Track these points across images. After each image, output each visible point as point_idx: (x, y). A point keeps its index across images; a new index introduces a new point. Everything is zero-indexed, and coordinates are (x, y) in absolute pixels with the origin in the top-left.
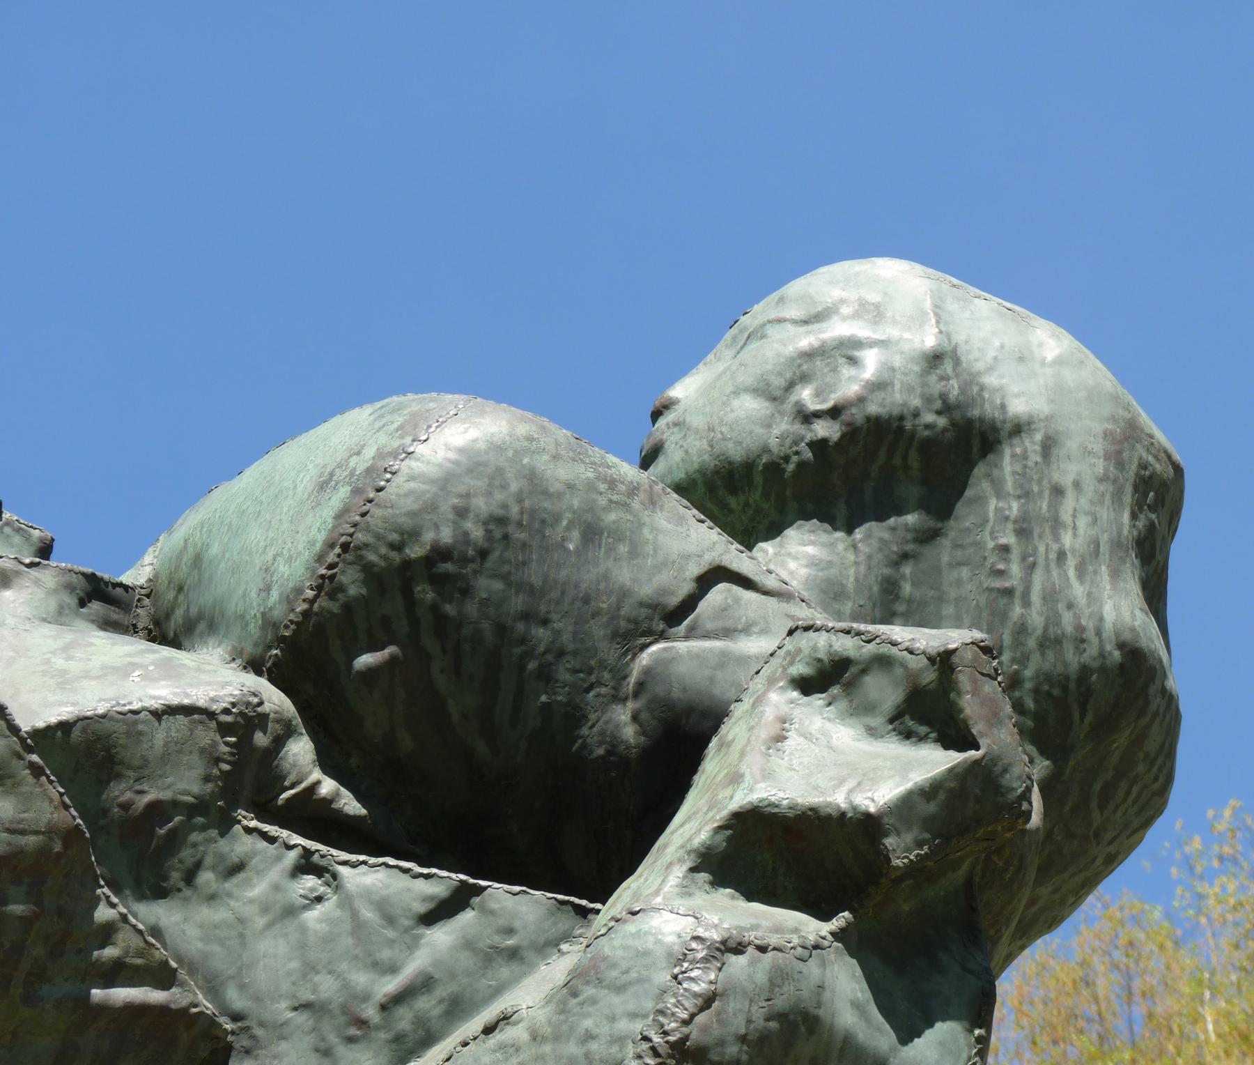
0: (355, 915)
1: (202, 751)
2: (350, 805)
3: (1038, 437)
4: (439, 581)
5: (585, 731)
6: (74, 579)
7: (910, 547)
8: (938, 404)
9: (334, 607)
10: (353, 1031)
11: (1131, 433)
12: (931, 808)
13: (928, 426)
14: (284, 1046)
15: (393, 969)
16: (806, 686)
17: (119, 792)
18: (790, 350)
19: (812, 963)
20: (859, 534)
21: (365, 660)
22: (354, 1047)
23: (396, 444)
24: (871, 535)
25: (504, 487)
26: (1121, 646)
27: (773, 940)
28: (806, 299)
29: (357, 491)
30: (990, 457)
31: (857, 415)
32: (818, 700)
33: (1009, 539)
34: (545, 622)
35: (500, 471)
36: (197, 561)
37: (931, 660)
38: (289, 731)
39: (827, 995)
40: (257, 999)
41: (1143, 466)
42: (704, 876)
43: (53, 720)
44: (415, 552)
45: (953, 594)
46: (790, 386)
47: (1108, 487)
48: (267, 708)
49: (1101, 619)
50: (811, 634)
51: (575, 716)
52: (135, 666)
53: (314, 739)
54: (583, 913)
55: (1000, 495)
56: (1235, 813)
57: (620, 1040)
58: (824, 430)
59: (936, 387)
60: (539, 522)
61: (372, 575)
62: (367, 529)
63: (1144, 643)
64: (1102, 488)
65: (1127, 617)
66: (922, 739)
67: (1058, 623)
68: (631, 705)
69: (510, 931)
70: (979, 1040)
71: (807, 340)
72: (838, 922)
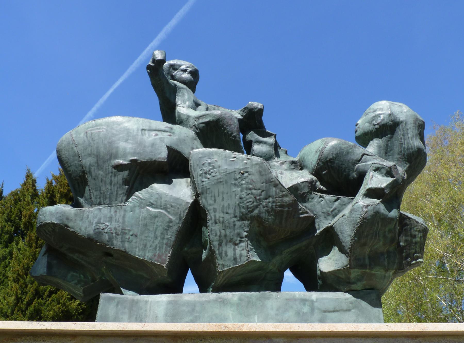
0: (327, 202)
1: (307, 186)
2: (325, 189)
3: (404, 123)
4: (331, 162)
5: (350, 176)
6: (290, 162)
7: (389, 139)
8: (391, 121)
9: (319, 167)
10: (328, 215)
11: (417, 119)
12: (390, 186)
13: (390, 124)
14: (321, 217)
15: (331, 208)
16: (375, 171)
17: (299, 192)
18: (371, 116)
19: (378, 205)
20: (383, 139)
21: (324, 172)
22: (329, 216)
23: (324, 146)
24: (384, 139)
25: (337, 150)
26: (417, 148)
27: (373, 204)
28: (373, 109)
29: (320, 153)
30: (398, 126)
31: (381, 124)
32: (376, 172)
33: (402, 137)
34: (344, 165)
35: (336, 148)
36: (304, 158)
37: (389, 167)
38: (316, 182)
39: (380, 209)
40: (317, 212)
41: (419, 123)
42: (365, 197)
43: (291, 186)
44: (328, 159)
45: (395, 144)
46: (372, 121)
47: (414, 128)
48: (314, 180)
49: (414, 145)
50: (375, 164)
51: (349, 175)
52: (298, 177)
53: (319, 182)
54: (352, 199)
55: (400, 131)
56: (458, 112)
57: (357, 217)
58: (377, 126)
59: (390, 119)
60: (342, 153)
61: (323, 163)
62: (322, 157)
63: (420, 147)
64: (413, 128)
65: (418, 144)
66: (389, 177)
67: (409, 147)
68: (355, 172)
69: (344, 202)
70: (398, 211)
71: (373, 115)
72: (380, 200)
